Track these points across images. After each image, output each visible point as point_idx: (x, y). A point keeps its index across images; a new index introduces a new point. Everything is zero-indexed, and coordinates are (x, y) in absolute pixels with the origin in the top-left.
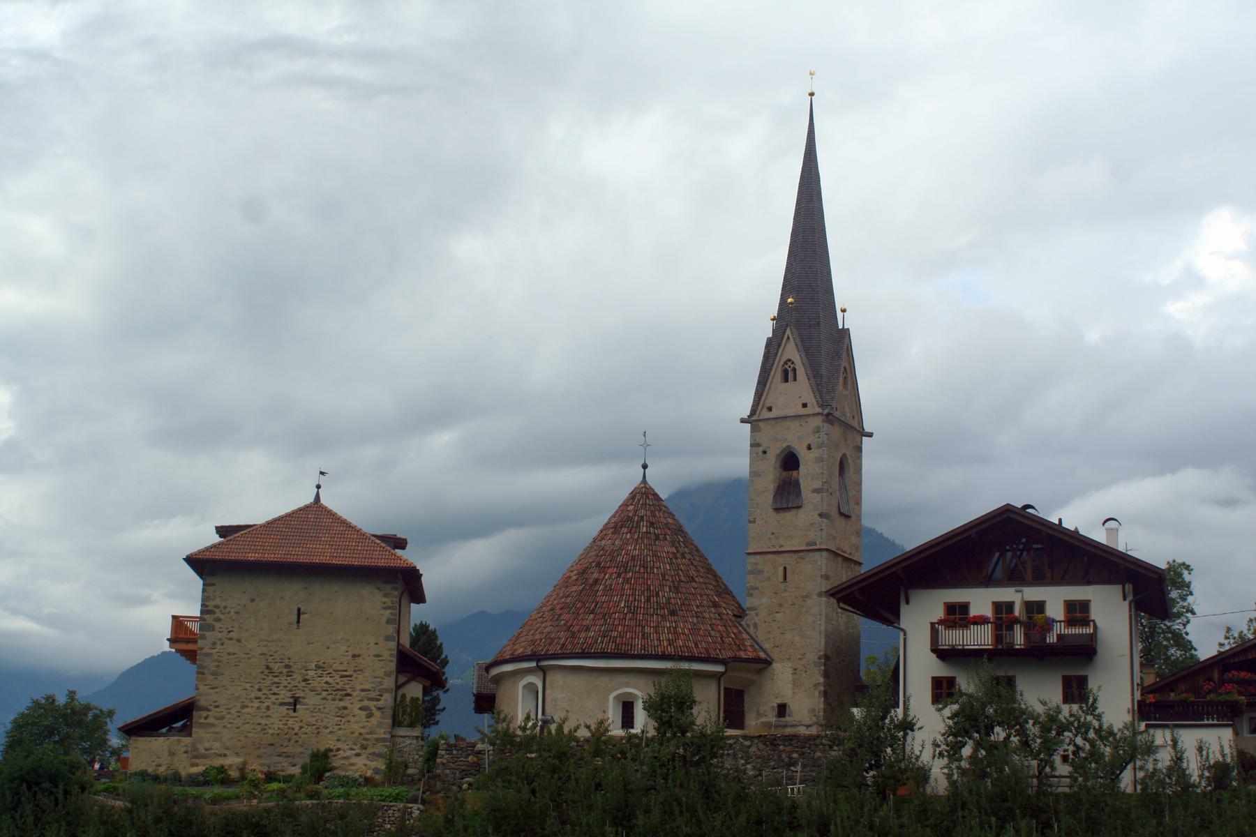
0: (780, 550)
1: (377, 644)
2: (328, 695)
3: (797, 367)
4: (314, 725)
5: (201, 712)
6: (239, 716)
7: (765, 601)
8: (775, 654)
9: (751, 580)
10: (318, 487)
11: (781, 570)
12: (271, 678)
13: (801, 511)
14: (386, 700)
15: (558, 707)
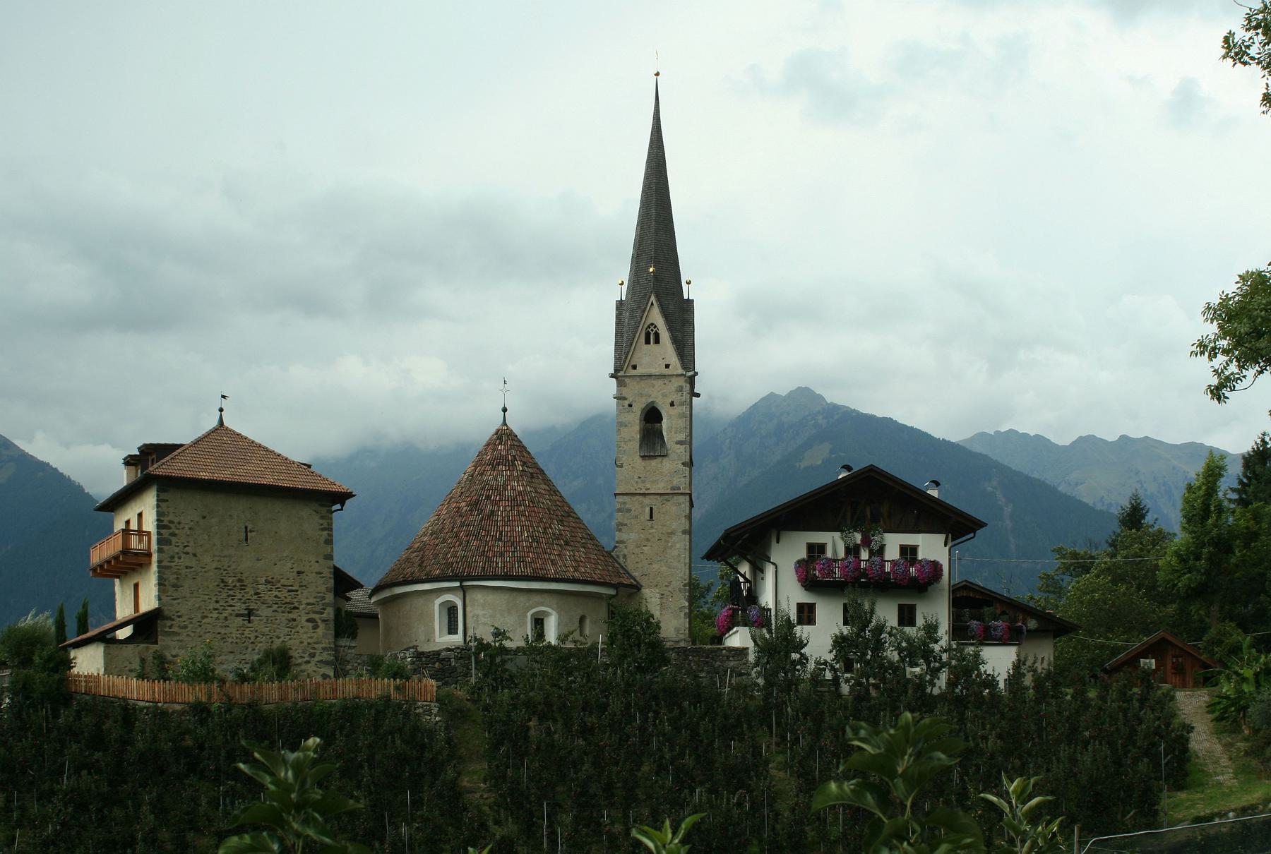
0: (647, 492)
1: (317, 562)
2: (279, 607)
4: (268, 635)
5: (166, 621)
6: (200, 626)
7: (633, 535)
8: (643, 582)
9: (619, 517)
10: (221, 410)
11: (648, 510)
12: (226, 591)
13: (665, 460)
14: (329, 614)
15: (480, 622)
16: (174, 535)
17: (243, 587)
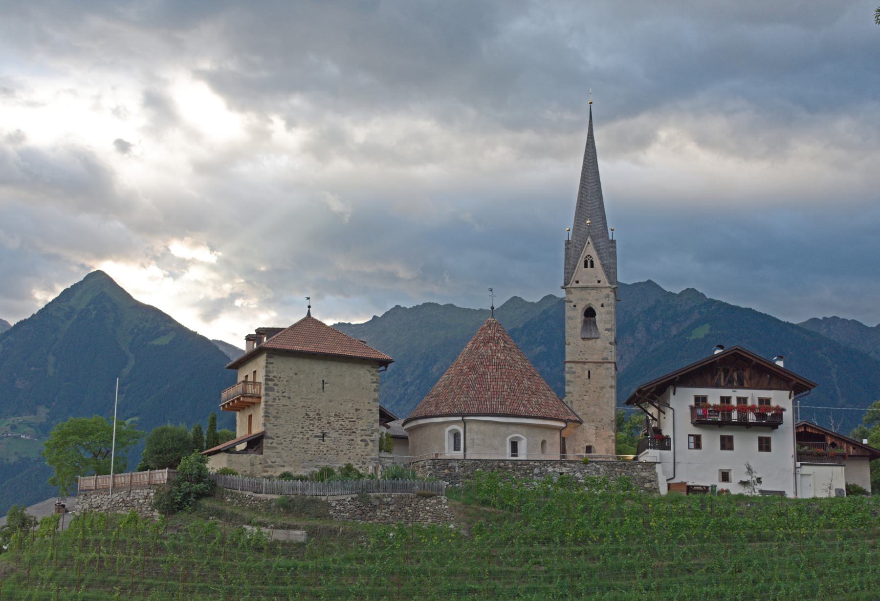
3: (594, 260)
8: (584, 418)
11: (587, 373)
17: (320, 419)
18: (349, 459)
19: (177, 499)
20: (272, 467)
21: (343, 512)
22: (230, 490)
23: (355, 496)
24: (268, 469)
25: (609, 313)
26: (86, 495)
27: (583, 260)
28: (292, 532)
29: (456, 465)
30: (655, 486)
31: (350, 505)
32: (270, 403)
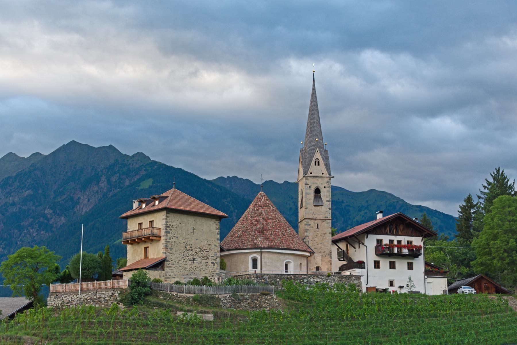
8: (315, 251)
11: (316, 225)
16: (171, 230)
17: (192, 250)
18: (206, 273)
19: (135, 297)
20: (169, 278)
21: (226, 304)
22: (162, 292)
23: (231, 294)
24: (167, 279)
25: (328, 191)
26: (57, 295)
27: (314, 161)
28: (206, 315)
29: (267, 277)
30: (360, 289)
31: (229, 299)
32: (168, 240)
